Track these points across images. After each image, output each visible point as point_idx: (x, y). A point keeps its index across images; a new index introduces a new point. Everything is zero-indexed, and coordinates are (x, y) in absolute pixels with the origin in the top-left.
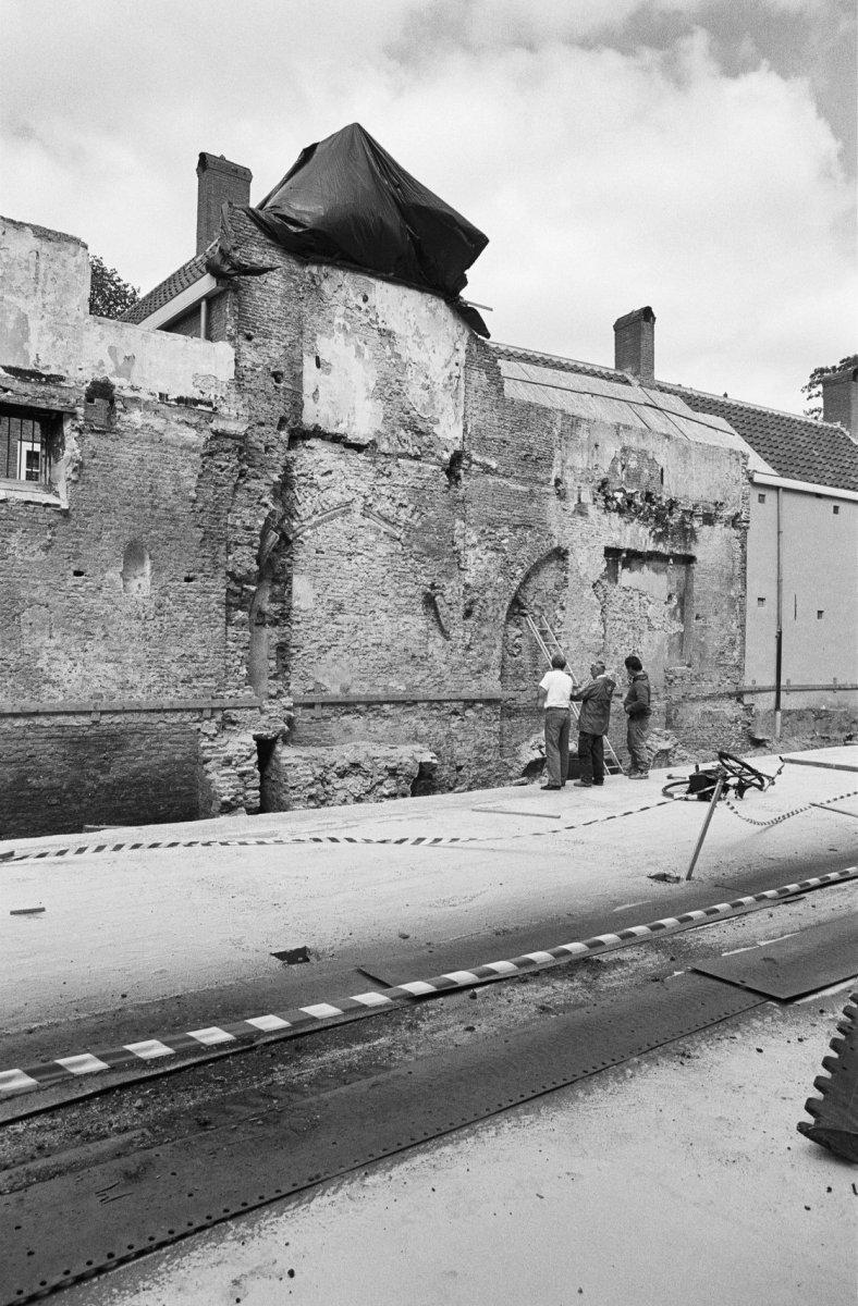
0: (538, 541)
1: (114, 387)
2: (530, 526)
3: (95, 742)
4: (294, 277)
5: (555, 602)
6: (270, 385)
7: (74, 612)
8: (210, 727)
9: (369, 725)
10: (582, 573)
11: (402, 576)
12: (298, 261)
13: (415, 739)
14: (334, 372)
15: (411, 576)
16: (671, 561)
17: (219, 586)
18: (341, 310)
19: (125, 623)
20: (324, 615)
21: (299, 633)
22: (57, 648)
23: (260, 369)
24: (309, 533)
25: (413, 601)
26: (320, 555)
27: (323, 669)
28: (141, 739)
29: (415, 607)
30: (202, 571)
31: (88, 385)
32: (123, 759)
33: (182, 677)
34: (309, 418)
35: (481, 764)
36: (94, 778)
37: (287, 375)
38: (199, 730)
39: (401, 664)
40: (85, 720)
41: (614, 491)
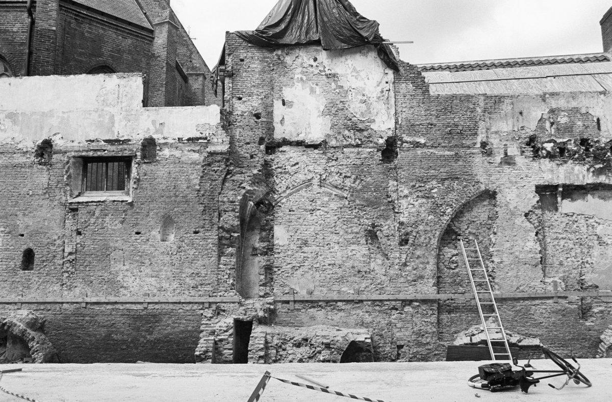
0: (465, 187)
1: (155, 139)
2: (457, 178)
3: (146, 319)
4: (266, 60)
5: (489, 229)
6: (253, 121)
8: (208, 313)
9: (327, 315)
10: (511, 207)
11: (348, 221)
13: (362, 325)
15: (356, 220)
17: (213, 236)
18: (299, 70)
19: (161, 257)
20: (295, 248)
21: (278, 259)
22: (127, 270)
23: (246, 114)
24: (284, 200)
25: (358, 236)
26: (292, 213)
28: (169, 318)
29: (359, 240)
30: (203, 227)
31: (142, 141)
32: (159, 328)
33: (192, 285)
34: (278, 135)
35: (419, 344)
36: (145, 337)
37: (263, 114)
38: (202, 314)
39: (350, 276)
40: (140, 307)
41: (543, 143)
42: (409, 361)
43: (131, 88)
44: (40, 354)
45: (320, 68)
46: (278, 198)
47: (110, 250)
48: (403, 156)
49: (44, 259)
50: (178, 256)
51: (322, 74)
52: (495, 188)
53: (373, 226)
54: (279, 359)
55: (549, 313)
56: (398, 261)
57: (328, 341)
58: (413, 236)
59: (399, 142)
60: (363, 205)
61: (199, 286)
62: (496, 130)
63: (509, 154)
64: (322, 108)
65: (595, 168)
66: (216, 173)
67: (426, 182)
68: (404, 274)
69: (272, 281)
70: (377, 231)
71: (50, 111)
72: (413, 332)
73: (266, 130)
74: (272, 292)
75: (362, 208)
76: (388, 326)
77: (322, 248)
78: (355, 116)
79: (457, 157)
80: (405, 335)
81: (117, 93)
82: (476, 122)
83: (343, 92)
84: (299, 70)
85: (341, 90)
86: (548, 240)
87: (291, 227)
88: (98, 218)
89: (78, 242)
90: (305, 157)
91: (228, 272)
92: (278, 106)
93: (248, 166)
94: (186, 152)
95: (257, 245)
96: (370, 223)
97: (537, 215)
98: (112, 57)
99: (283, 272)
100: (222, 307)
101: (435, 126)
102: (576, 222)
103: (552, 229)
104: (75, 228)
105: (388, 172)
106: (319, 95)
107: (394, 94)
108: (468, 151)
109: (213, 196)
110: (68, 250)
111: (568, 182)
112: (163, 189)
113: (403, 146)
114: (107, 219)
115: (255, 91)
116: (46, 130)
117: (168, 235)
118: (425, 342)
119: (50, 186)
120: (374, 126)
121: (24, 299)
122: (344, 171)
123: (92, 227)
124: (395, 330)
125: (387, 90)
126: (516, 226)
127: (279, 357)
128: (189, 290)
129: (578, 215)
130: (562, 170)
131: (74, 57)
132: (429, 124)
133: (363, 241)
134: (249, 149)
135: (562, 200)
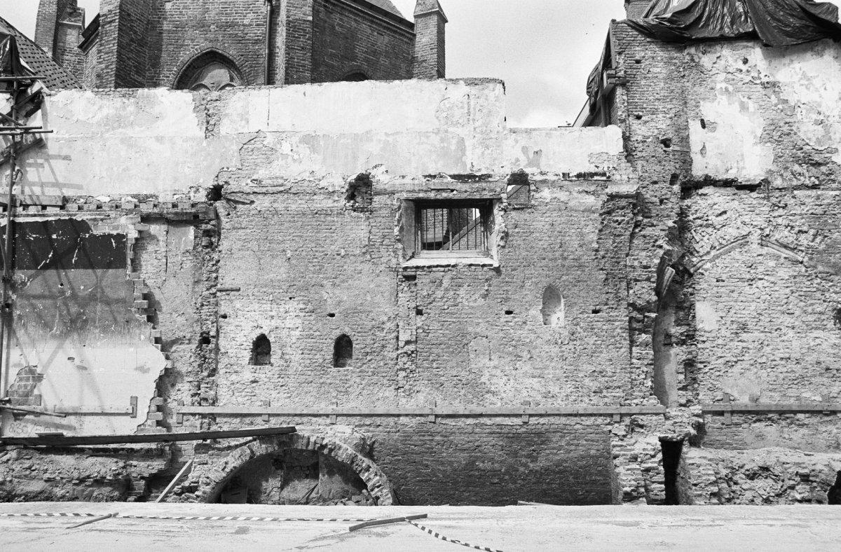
1: (527, 175)
3: (527, 438)
4: (674, 61)
6: (660, 150)
7: (507, 341)
8: (620, 429)
9: (782, 432)
14: (719, 129)
15: (818, 295)
17: (622, 315)
18: (722, 76)
19: (546, 348)
20: (728, 334)
21: (704, 351)
22: (495, 367)
23: (650, 140)
25: (823, 317)
26: (721, 284)
27: (731, 381)
28: (561, 437)
29: (825, 323)
30: (606, 304)
31: (508, 177)
32: (548, 452)
33: (593, 390)
34: (698, 171)
36: (525, 465)
37: (675, 140)
38: (610, 431)
43: (486, 99)
44: (385, 491)
45: (752, 75)
47: (468, 337)
49: (368, 350)
50: (571, 346)
61: (604, 391)
64: (759, 132)
66: (619, 224)
71: (367, 132)
73: (680, 163)
75: (826, 277)
77: (769, 334)
78: (807, 144)
81: (466, 106)
84: (722, 76)
88: (447, 290)
89: (419, 325)
90: (736, 202)
91: (645, 369)
94: (575, 194)
98: (367, 60)
100: (640, 421)
104: (414, 305)
109: (619, 258)
110: (404, 337)
112: (544, 249)
114: (462, 292)
115: (660, 107)
116: (362, 160)
117: (549, 315)
119: (371, 243)
121: (340, 410)
122: (797, 224)
123: (439, 304)
128: (589, 396)
131: (324, 61)
133: (830, 324)
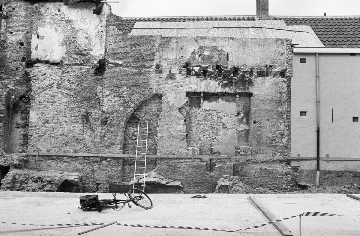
2: (139, 86)
4: (29, 9)
5: (158, 117)
6: (18, 47)
9: (57, 164)
10: (170, 104)
11: (73, 109)
12: (30, 3)
13: (77, 171)
14: (45, 39)
15: (77, 109)
16: (238, 96)
18: (49, 17)
20: (41, 124)
21: (31, 131)
23: (15, 43)
24: (37, 96)
25: (77, 118)
26: (41, 103)
27: (40, 143)
29: (78, 121)
34: (34, 56)
37: (25, 43)
41: (193, 67)
42: (103, 192)
45: (62, 16)
46: (34, 94)
48: (108, 72)
51: (63, 20)
52: (161, 92)
53: (87, 113)
54: (22, 189)
55: (189, 167)
56: (100, 134)
57: (50, 179)
58: (110, 119)
59: (107, 63)
60: (81, 100)
62: (166, 58)
63: (172, 73)
64: (61, 41)
65: (223, 83)
67: (120, 87)
68: (103, 141)
69: (27, 144)
70: (89, 116)
72: (106, 176)
74: (27, 150)
75: (81, 102)
76: (92, 172)
77: (56, 125)
78: (81, 47)
79: (140, 73)
80: (101, 178)
82: (154, 52)
83: (75, 31)
84: (49, 17)
85: (74, 30)
86: (194, 125)
87: (40, 112)
90: (50, 70)
92: (34, 38)
93: (14, 74)
95: (19, 122)
96: (85, 111)
97: (186, 110)
99: (34, 138)
101: (129, 54)
102: (211, 114)
103: (196, 118)
105: (98, 81)
106: (60, 33)
107: (105, 34)
108: (147, 70)
111: (206, 91)
113: (109, 65)
118: (113, 182)
120: (91, 53)
122: (72, 79)
124: (95, 174)
125: (101, 31)
126: (172, 116)
127: (22, 188)
129: (212, 110)
130: (203, 83)
132: (125, 52)
133: (80, 121)
134: (15, 64)
135: (204, 101)
